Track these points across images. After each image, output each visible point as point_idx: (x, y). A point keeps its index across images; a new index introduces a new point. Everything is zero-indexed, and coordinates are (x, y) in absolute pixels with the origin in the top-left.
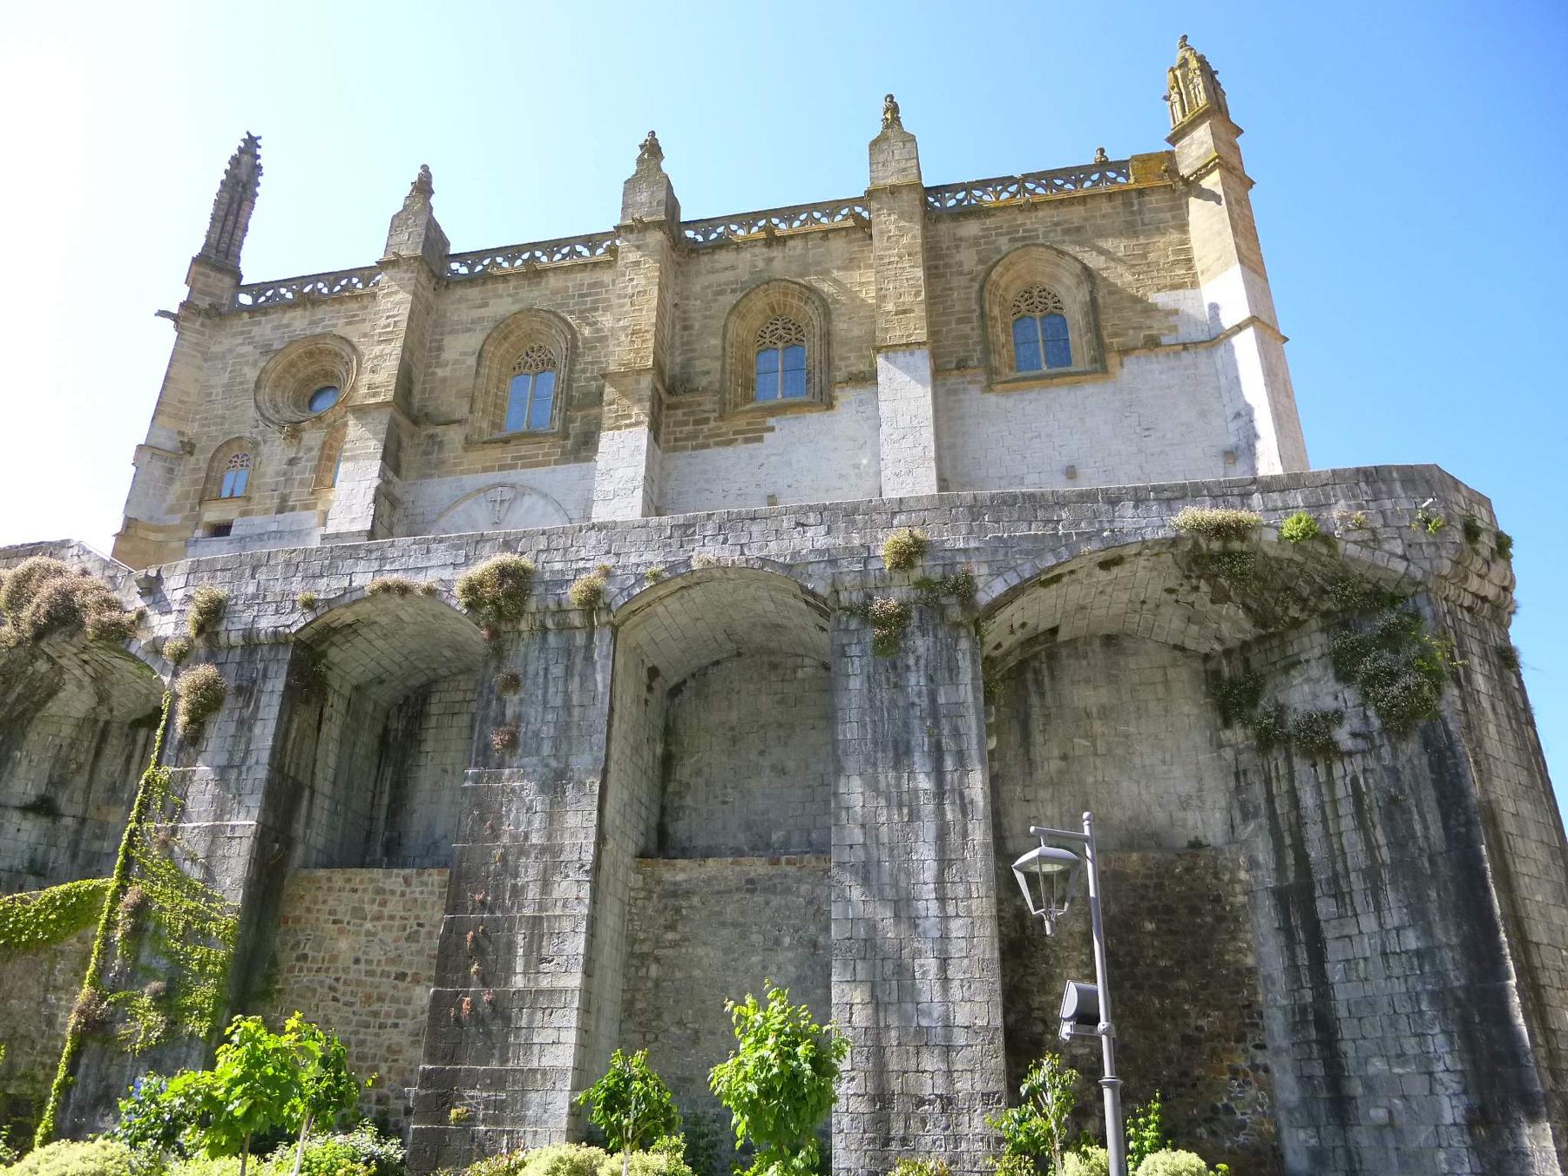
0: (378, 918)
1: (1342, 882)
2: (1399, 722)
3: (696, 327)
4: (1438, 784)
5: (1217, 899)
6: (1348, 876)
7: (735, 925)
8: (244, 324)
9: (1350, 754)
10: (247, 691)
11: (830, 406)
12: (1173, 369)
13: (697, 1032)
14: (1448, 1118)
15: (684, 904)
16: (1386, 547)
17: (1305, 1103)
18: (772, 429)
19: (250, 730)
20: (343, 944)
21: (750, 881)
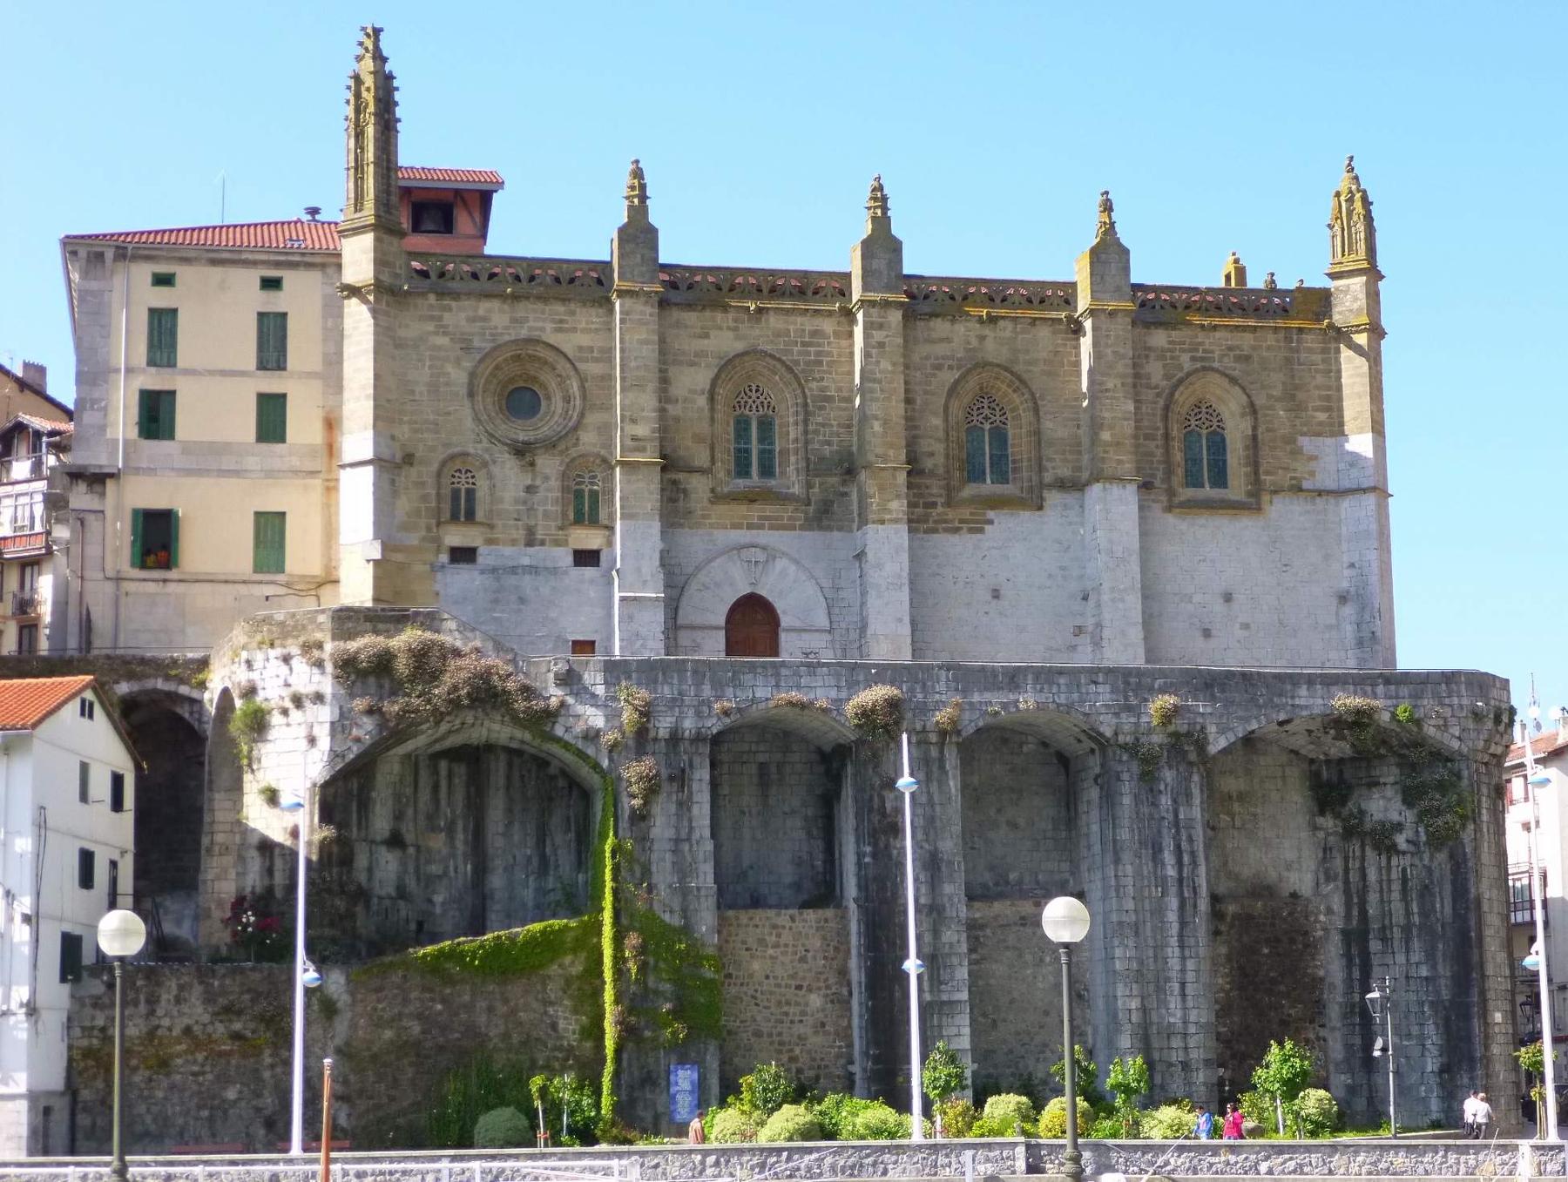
0: (776, 946)
1: (1388, 932)
2: (1437, 841)
3: (919, 402)
4: (1454, 882)
5: (1306, 933)
6: (1391, 929)
7: (1015, 948)
8: (431, 307)
9: (1404, 853)
10: (680, 779)
11: (1040, 508)
12: (1308, 512)
13: (994, 1021)
14: (1429, 1069)
15: (981, 933)
16: (1451, 731)
17: (1347, 1060)
18: (991, 522)
19: (689, 810)
20: (756, 966)
21: (1023, 918)
